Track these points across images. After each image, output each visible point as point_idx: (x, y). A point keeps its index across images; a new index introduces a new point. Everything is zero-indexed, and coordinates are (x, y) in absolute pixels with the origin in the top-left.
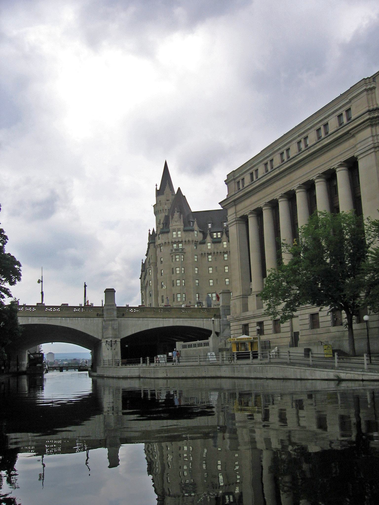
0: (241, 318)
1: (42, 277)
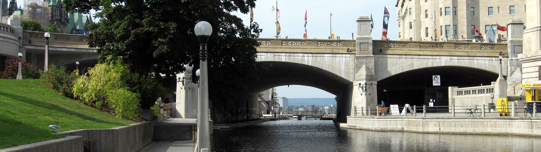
0: (537, 57)
1: (277, 2)
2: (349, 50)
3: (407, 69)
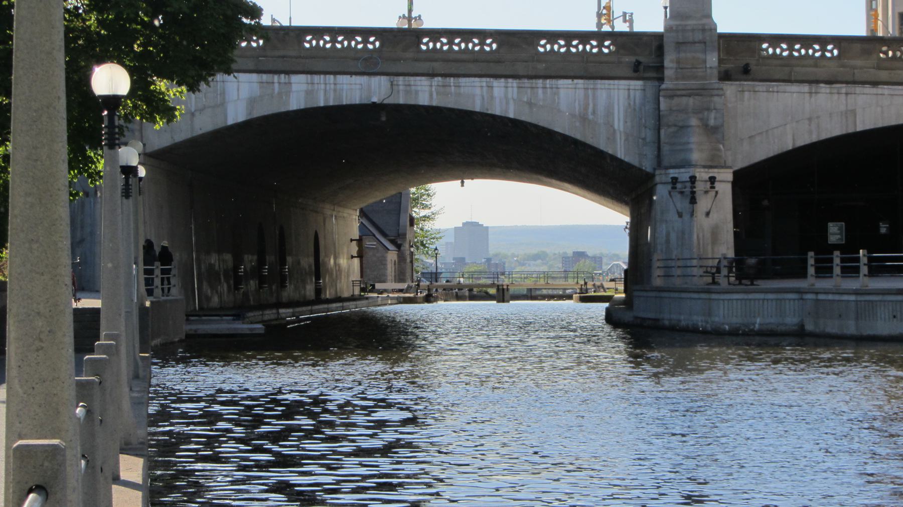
1: (290, 18)
2: (641, 68)
3: (833, 129)
